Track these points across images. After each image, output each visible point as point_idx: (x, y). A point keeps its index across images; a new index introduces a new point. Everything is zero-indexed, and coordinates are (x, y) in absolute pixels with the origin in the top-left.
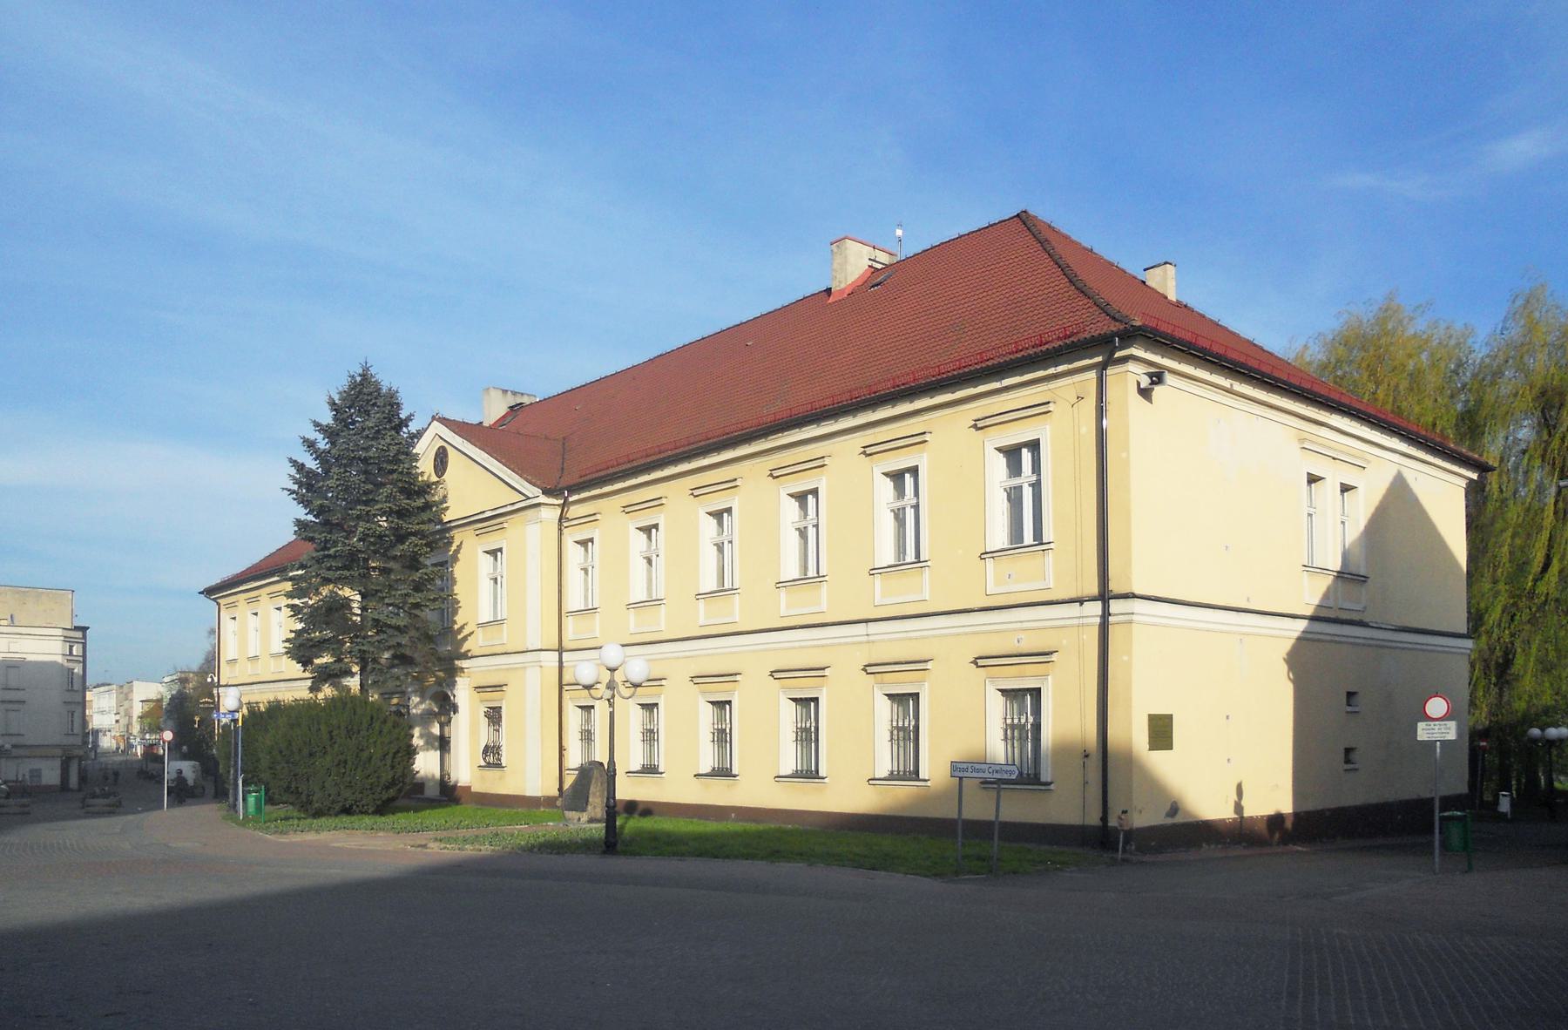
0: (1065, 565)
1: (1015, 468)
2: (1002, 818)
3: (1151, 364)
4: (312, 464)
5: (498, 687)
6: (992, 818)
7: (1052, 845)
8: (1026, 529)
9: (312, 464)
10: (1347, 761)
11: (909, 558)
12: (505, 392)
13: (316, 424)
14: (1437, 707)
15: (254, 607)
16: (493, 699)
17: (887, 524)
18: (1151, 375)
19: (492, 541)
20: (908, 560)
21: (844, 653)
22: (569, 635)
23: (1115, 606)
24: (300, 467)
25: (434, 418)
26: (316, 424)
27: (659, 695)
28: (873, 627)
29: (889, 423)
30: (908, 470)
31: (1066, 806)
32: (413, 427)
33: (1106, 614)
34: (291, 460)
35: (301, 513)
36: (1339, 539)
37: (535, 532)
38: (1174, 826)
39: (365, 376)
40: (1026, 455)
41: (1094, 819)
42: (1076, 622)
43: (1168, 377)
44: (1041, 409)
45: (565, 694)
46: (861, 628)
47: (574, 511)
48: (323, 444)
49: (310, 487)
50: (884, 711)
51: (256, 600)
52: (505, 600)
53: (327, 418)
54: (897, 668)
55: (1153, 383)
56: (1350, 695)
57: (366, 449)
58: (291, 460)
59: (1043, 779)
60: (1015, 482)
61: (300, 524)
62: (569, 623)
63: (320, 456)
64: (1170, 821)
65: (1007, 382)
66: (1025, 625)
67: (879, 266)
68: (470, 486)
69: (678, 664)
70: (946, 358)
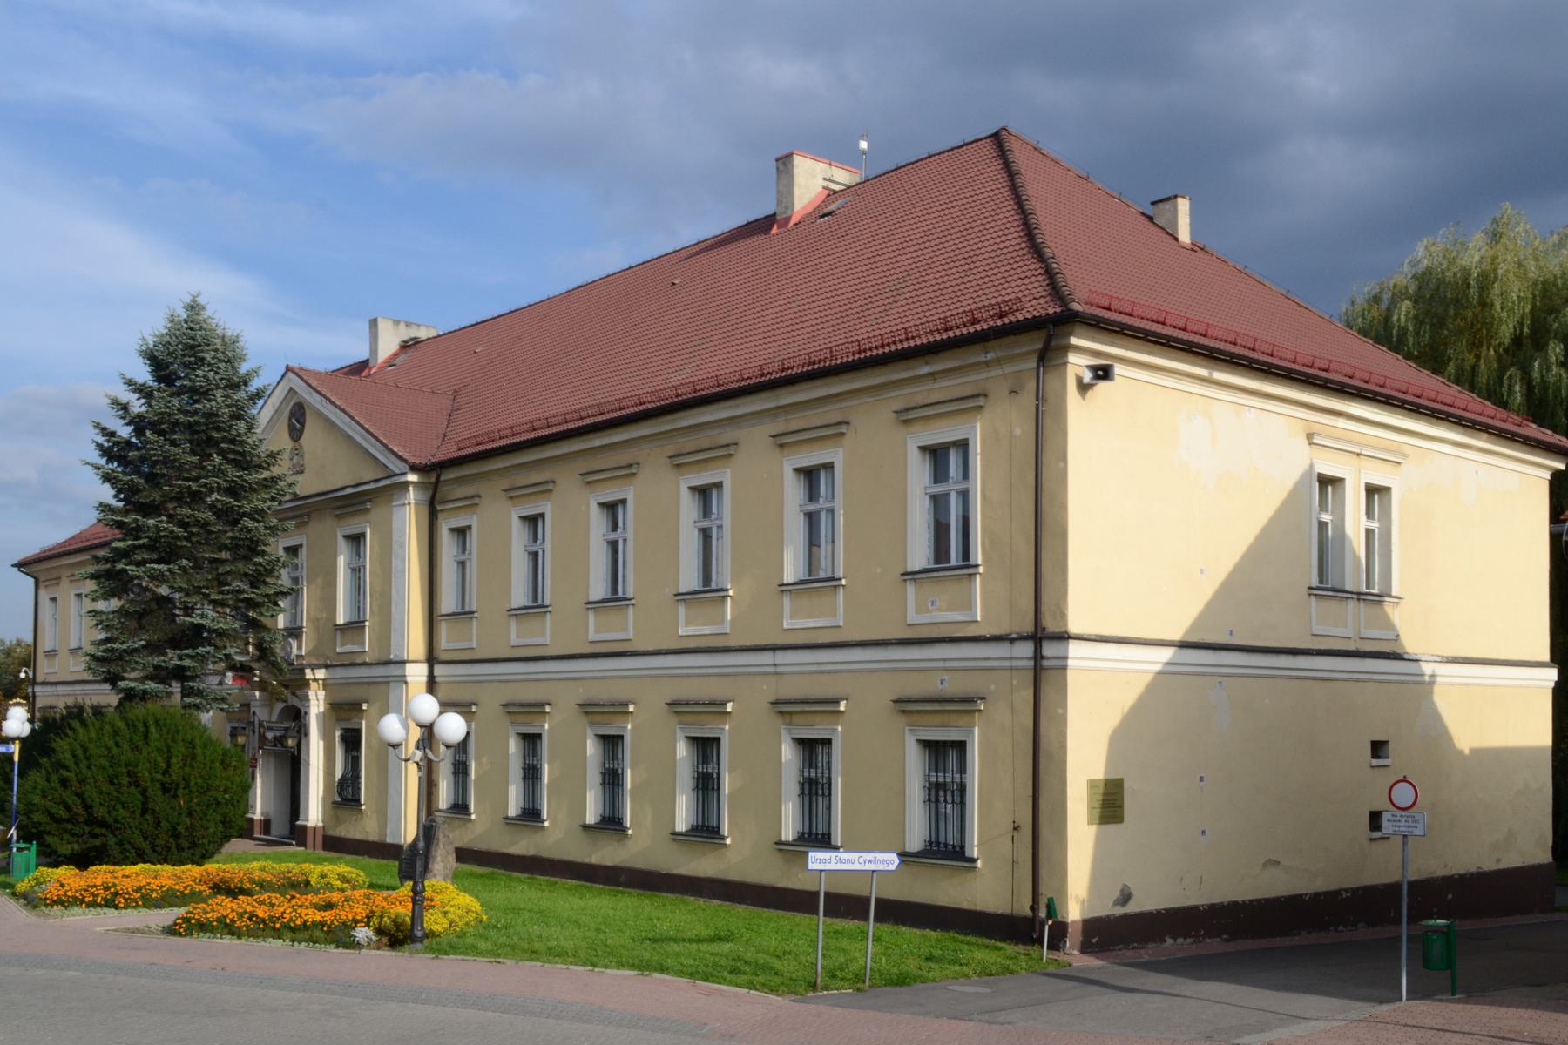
1: (940, 474)
3: (1097, 354)
4: (125, 432)
8: (949, 551)
9: (125, 432)
11: (708, 591)
12: (397, 323)
13: (130, 383)
17: (795, 528)
19: (353, 526)
20: (953, 562)
21: (563, 690)
22: (444, 641)
23: (438, 670)
24: (98, 445)
25: (288, 369)
26: (130, 383)
30: (956, 444)
32: (254, 386)
33: (1038, 656)
34: (97, 425)
35: (107, 494)
36: (96, 687)
38: (1125, 917)
39: (194, 307)
40: (954, 459)
42: (1007, 664)
43: (1119, 369)
46: (766, 658)
48: (138, 406)
49: (123, 460)
50: (915, 765)
52: (630, 544)
53: (143, 374)
55: (1097, 377)
58: (97, 425)
59: (968, 854)
60: (940, 489)
61: (104, 508)
62: (443, 630)
63: (139, 424)
64: (1119, 911)
66: (948, 664)
67: (837, 187)
69: (563, 690)
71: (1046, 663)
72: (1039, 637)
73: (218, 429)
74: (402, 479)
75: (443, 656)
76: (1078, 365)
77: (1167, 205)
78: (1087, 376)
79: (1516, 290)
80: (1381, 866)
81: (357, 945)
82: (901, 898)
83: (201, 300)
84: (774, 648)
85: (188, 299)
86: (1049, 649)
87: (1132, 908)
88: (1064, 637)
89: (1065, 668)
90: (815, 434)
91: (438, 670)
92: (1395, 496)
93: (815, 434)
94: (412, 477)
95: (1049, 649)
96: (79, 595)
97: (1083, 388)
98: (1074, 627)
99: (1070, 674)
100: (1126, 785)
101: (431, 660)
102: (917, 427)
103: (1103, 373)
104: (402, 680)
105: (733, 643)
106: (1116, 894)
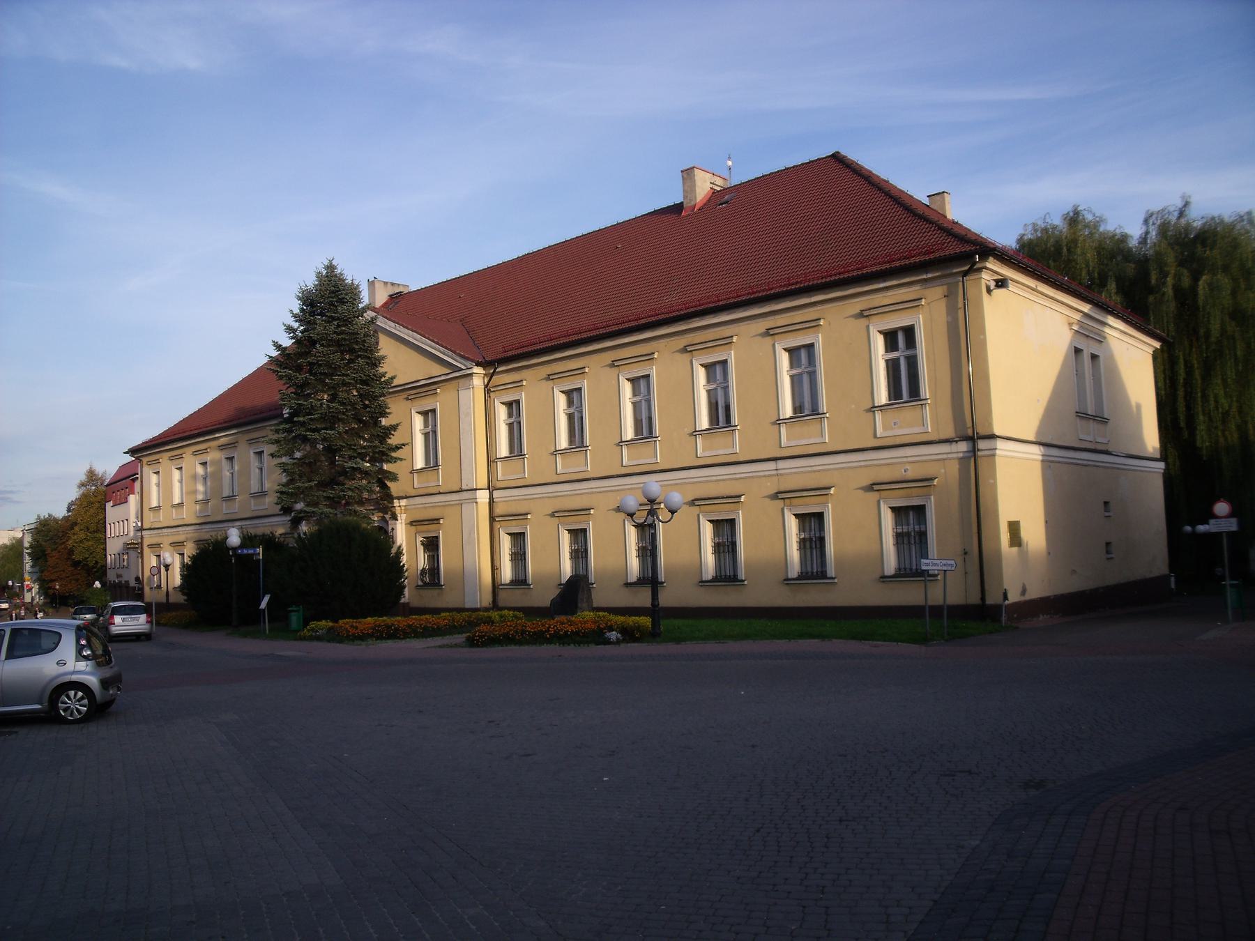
0: (931, 416)
2: (930, 603)
5: (435, 521)
6: (922, 603)
7: (943, 618)
10: (1108, 552)
14: (1222, 508)
15: (178, 463)
16: (430, 531)
18: (997, 281)
19: (426, 404)
20: (806, 412)
23: (496, 494)
27: (928, 496)
28: (781, 464)
29: (631, 347)
31: (953, 591)
37: (472, 401)
39: (331, 267)
40: (803, 354)
41: (974, 599)
43: (1011, 286)
44: (914, 304)
45: (497, 525)
46: (771, 465)
47: (497, 379)
51: (180, 457)
54: (805, 494)
56: (1106, 503)
57: (338, 326)
64: (1023, 599)
65: (814, 299)
68: (399, 361)
70: (673, 300)
71: (980, 453)
72: (972, 439)
73: (357, 343)
74: (469, 372)
75: (499, 485)
76: (986, 277)
77: (938, 198)
78: (992, 284)
79: (1091, 255)
80: (1114, 576)
81: (608, 642)
82: (904, 603)
83: (334, 263)
84: (775, 459)
85: (326, 263)
86: (982, 444)
87: (1027, 597)
88: (993, 437)
89: (994, 455)
90: (808, 325)
91: (496, 494)
92: (1101, 359)
93: (808, 325)
94: (477, 370)
95: (982, 444)
96: (260, 454)
97: (989, 291)
98: (997, 431)
99: (998, 459)
100: (1022, 524)
101: (491, 488)
102: (874, 319)
103: (1001, 283)
104: (474, 501)
105: (741, 459)
106: (1020, 590)
